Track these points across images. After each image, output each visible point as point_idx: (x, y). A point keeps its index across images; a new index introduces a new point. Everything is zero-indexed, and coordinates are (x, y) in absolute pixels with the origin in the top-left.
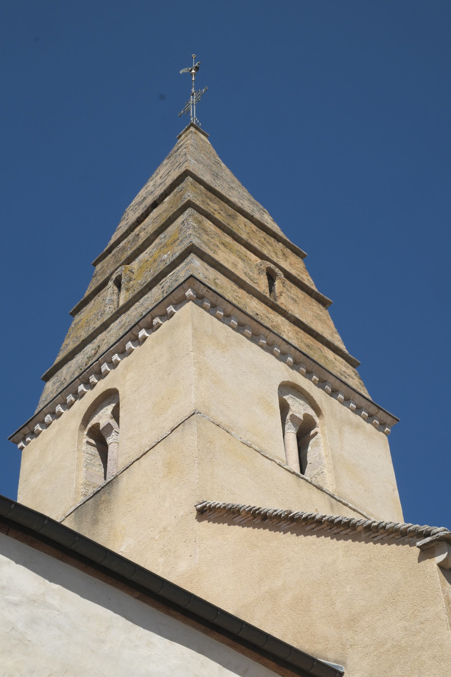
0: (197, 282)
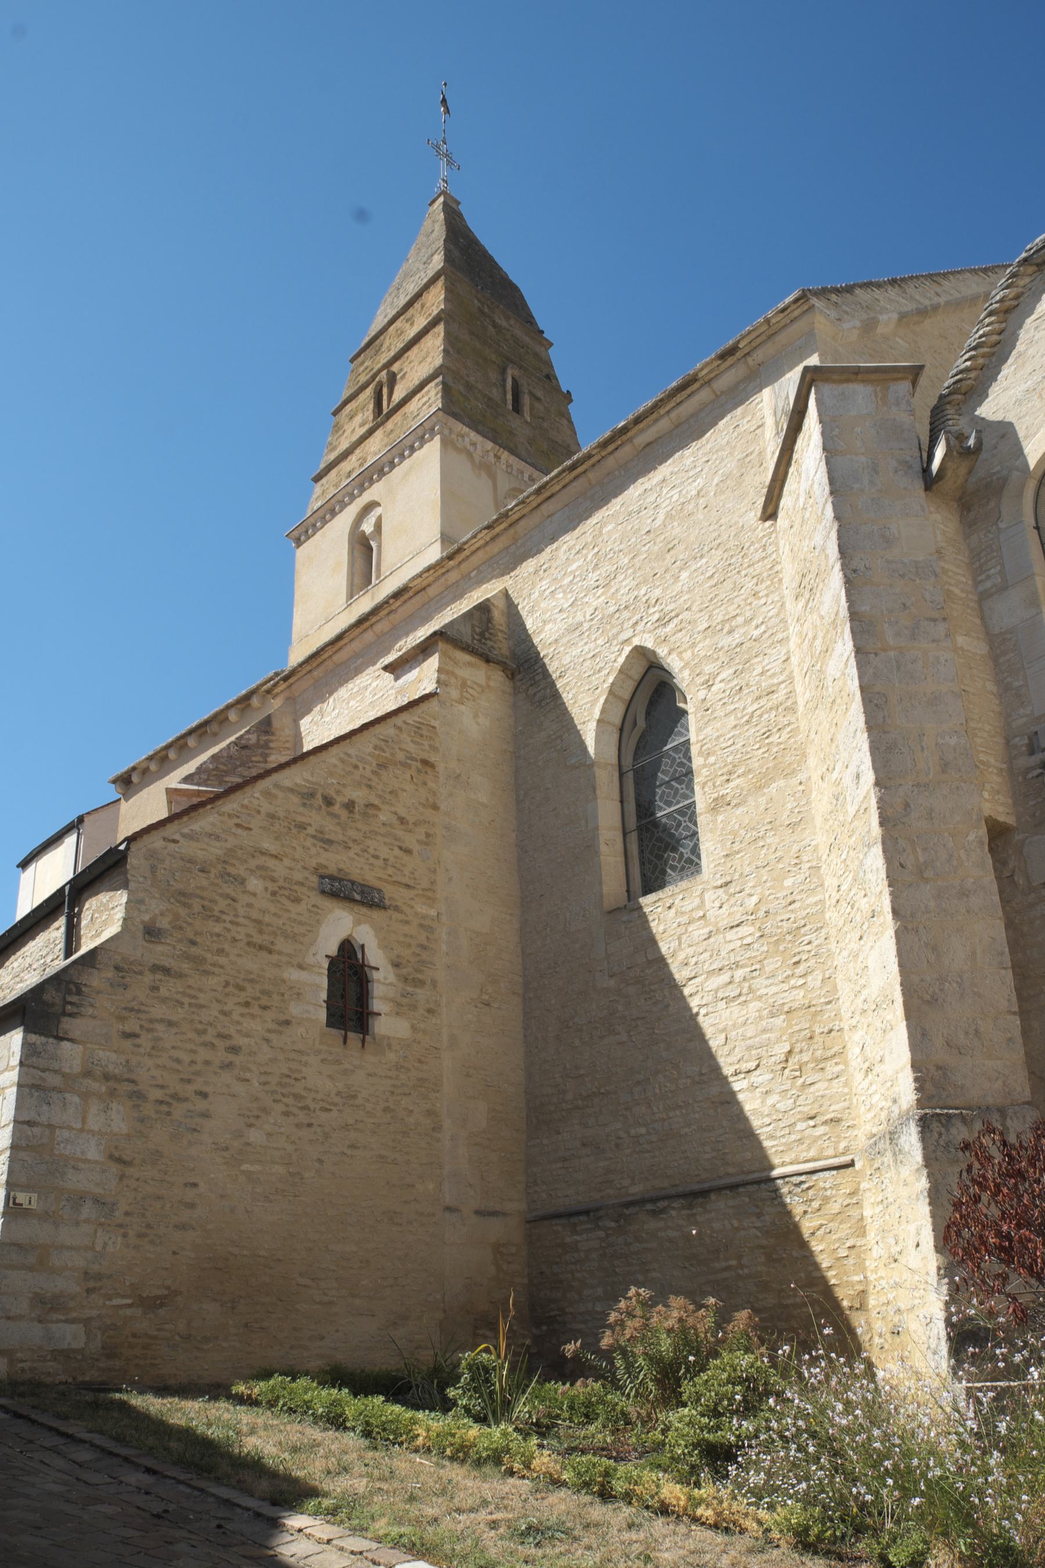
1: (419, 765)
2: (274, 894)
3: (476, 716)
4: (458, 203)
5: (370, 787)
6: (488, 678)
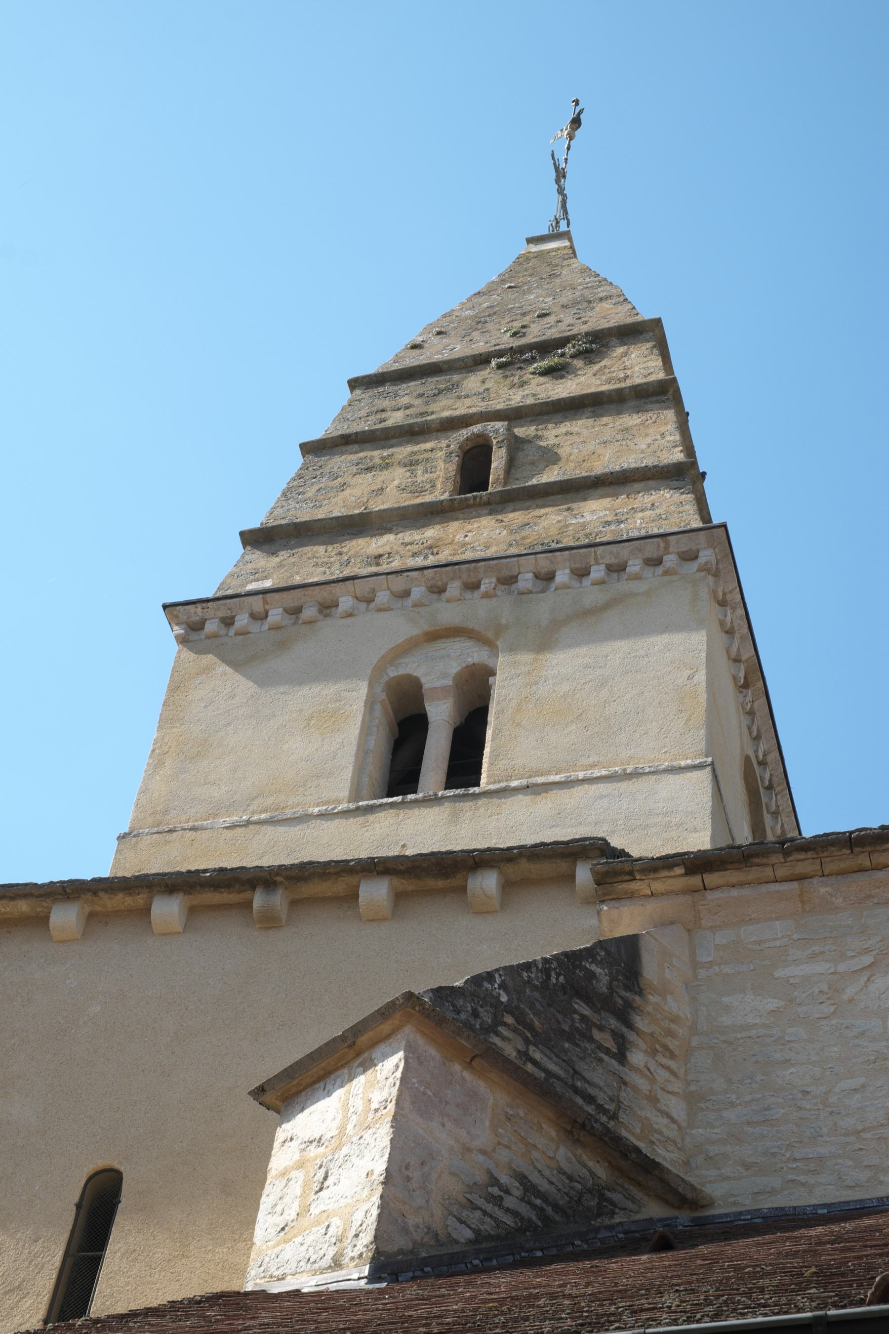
0: (178, 608)
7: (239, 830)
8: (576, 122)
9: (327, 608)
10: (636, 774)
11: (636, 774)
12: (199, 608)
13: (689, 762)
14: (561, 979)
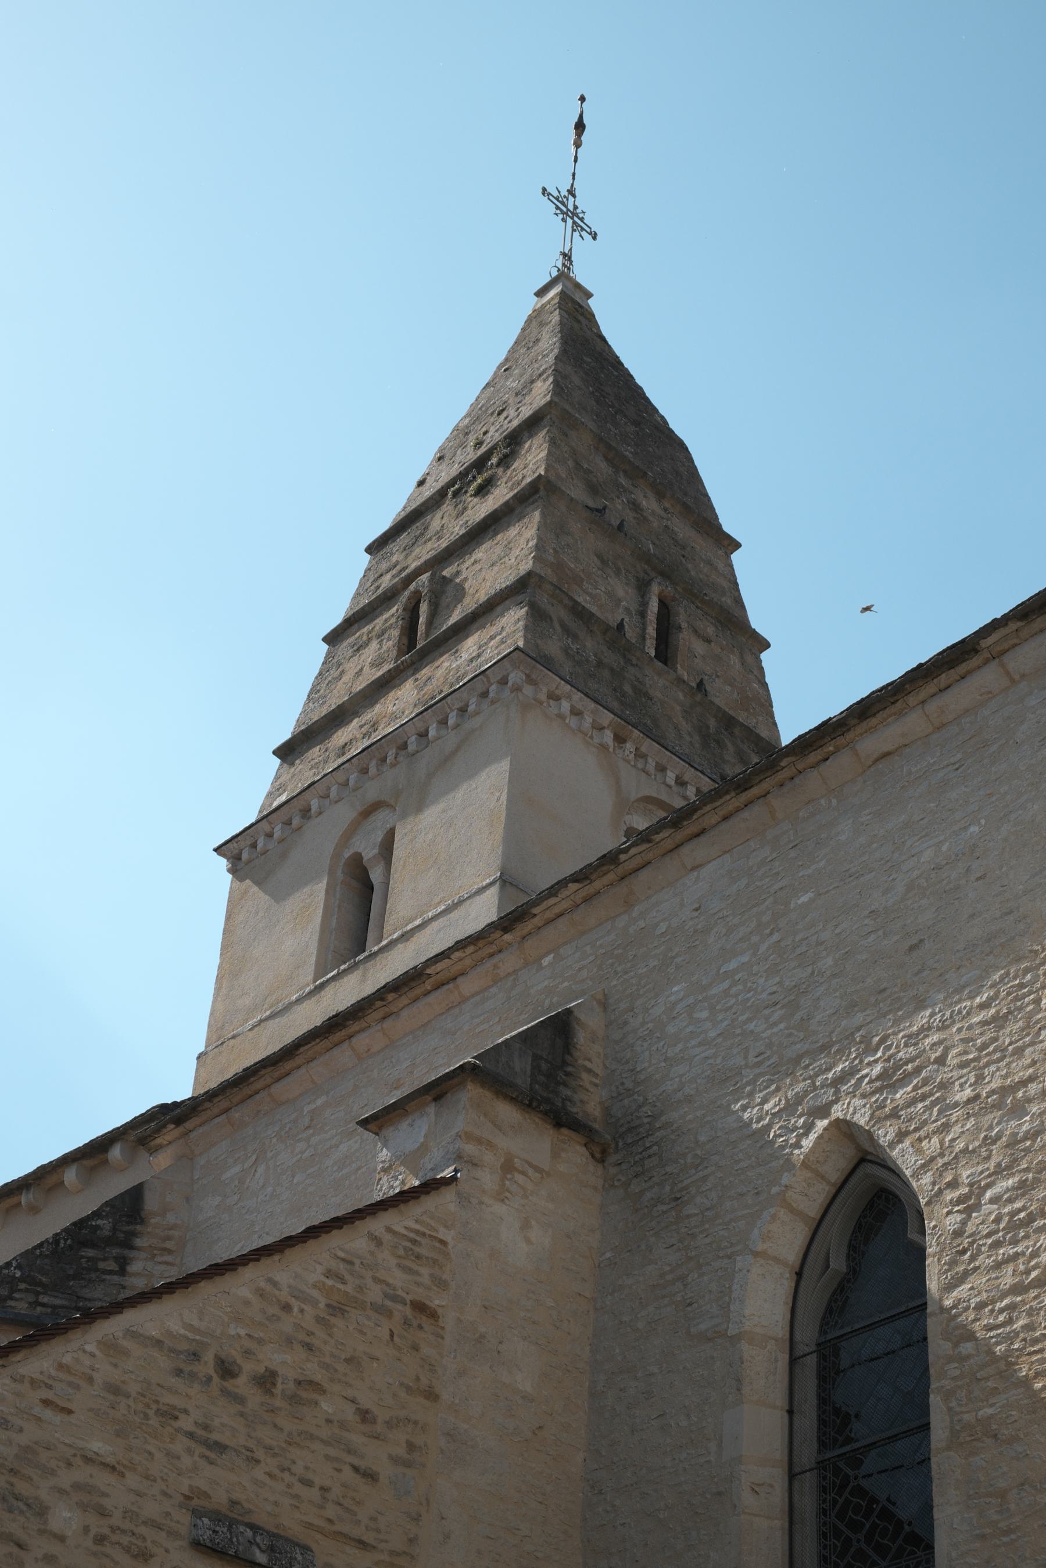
1: (408, 1311)
2: (100, 1540)
3: (525, 1226)
4: (589, 295)
5: (309, 1347)
6: (555, 1155)
7: (256, 1029)
8: (580, 127)
9: (306, 813)
10: (461, 902)
11: (461, 902)
12: (234, 844)
13: (488, 881)
14: (69, 1242)
